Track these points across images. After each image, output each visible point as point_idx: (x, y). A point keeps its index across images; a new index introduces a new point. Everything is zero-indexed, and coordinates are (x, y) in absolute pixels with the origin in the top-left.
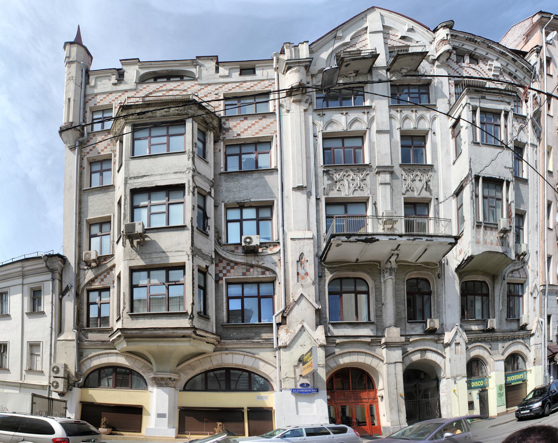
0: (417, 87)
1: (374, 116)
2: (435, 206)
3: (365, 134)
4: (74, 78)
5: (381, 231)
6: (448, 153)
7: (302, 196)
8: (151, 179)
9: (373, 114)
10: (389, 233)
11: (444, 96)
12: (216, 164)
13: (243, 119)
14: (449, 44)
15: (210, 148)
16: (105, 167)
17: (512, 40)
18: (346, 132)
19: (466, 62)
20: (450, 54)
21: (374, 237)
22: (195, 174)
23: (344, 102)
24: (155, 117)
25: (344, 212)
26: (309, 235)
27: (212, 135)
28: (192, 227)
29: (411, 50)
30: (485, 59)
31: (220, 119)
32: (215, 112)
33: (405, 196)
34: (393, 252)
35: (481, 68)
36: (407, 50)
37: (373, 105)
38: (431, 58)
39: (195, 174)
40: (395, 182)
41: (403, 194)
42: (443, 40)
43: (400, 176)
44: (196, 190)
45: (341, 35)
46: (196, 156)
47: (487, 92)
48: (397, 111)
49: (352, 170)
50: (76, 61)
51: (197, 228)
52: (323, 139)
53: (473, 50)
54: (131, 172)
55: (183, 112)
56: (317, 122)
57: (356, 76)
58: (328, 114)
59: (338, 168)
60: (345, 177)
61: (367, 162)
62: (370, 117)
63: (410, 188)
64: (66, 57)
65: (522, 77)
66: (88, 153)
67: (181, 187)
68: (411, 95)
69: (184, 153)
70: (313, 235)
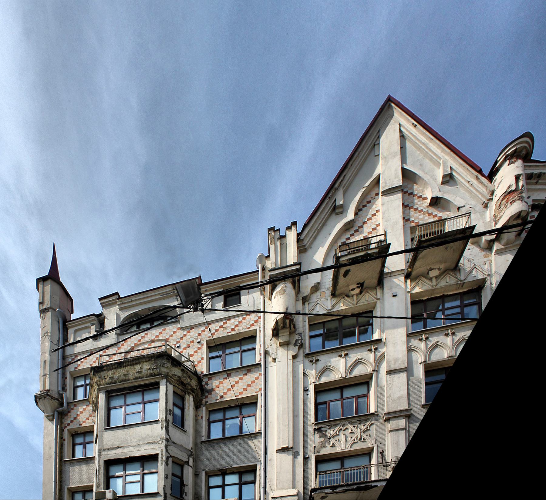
1: (384, 353)
4: (49, 334)
8: (125, 450)
9: (382, 350)
12: (197, 432)
13: (226, 376)
14: (521, 199)
16: (88, 439)
21: (371, 484)
22: (169, 443)
24: (129, 380)
27: (191, 399)
28: (165, 494)
29: (449, 227)
37: (384, 337)
42: (508, 193)
45: (341, 202)
46: (170, 424)
49: (351, 423)
50: (50, 308)
51: (171, 495)
54: (105, 443)
55: (155, 371)
56: (308, 371)
57: (361, 292)
62: (379, 354)
64: (40, 303)
66: (69, 424)
67: (154, 458)
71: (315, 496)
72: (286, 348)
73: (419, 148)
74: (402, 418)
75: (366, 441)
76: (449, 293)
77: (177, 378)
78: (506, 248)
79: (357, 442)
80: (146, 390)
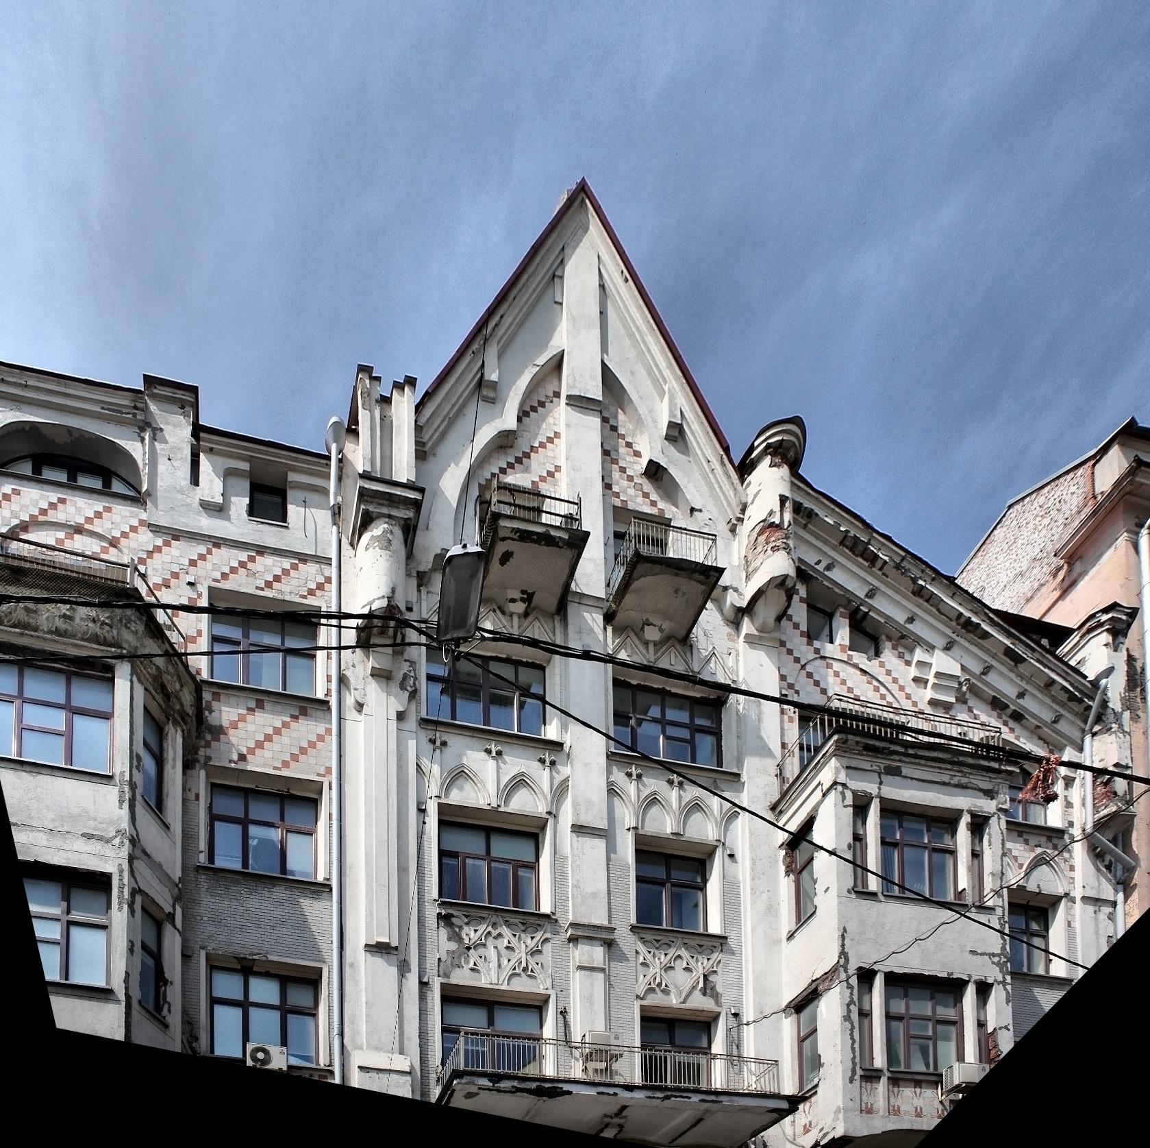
0: (687, 703)
1: (567, 780)
2: (729, 1030)
3: (543, 828)
5: (577, 1072)
6: (772, 910)
7: (386, 970)
9: (565, 770)
10: (598, 1079)
11: (764, 751)
13: (252, 704)
15: (174, 780)
17: (1008, 571)
18: (495, 812)
19: (838, 641)
20: (790, 593)
21: (560, 1085)
23: (495, 710)
24: (36, 629)
25: (484, 1022)
26: (402, 1063)
30: (905, 641)
31: (200, 687)
32: (186, 654)
33: (644, 1003)
34: (607, 1120)
35: (889, 673)
36: (662, 544)
37: (567, 740)
38: (732, 599)
39: (138, 853)
40: (618, 968)
41: (638, 997)
43: (630, 954)
44: (138, 898)
47: (907, 755)
48: (629, 775)
49: (509, 925)
51: (140, 1002)
52: (442, 823)
53: (861, 594)
55: (106, 633)
56: (425, 763)
58: (456, 742)
59: (473, 912)
60: (490, 939)
61: (545, 908)
62: (558, 779)
63: (659, 985)
65: (1048, 716)
68: (671, 731)
69: (110, 778)
70: (412, 1066)
71: (458, 1088)
72: (384, 685)
73: (631, 335)
74: (599, 943)
75: (535, 978)
76: (674, 690)
77: (153, 671)
78: (760, 638)
79: (519, 975)
80: (76, 674)
